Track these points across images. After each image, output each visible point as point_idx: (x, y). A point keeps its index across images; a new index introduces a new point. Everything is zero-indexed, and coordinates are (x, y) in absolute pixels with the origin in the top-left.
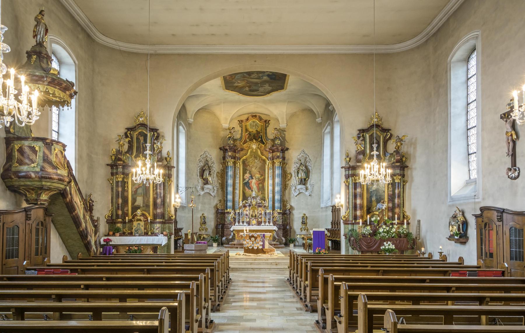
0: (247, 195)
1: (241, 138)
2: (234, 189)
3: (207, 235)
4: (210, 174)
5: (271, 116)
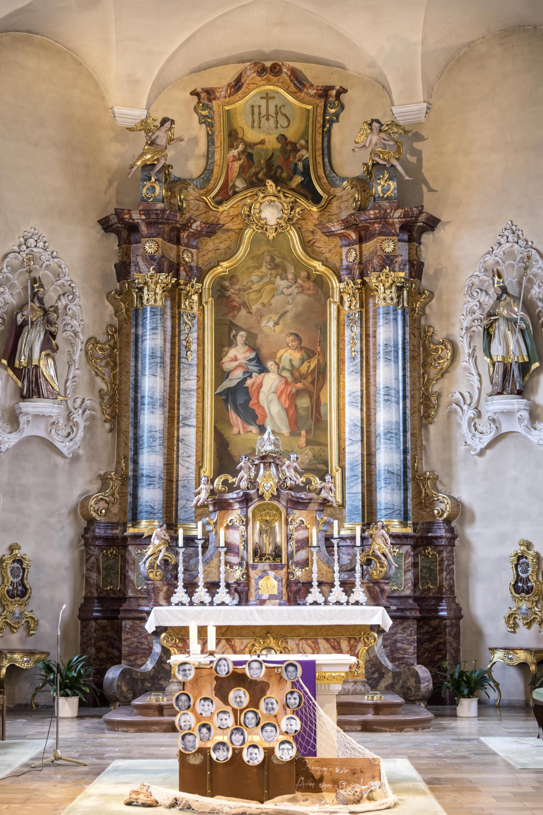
1: (208, 172)
2: (173, 420)
3: (30, 653)
4: (49, 344)
5: (352, 67)
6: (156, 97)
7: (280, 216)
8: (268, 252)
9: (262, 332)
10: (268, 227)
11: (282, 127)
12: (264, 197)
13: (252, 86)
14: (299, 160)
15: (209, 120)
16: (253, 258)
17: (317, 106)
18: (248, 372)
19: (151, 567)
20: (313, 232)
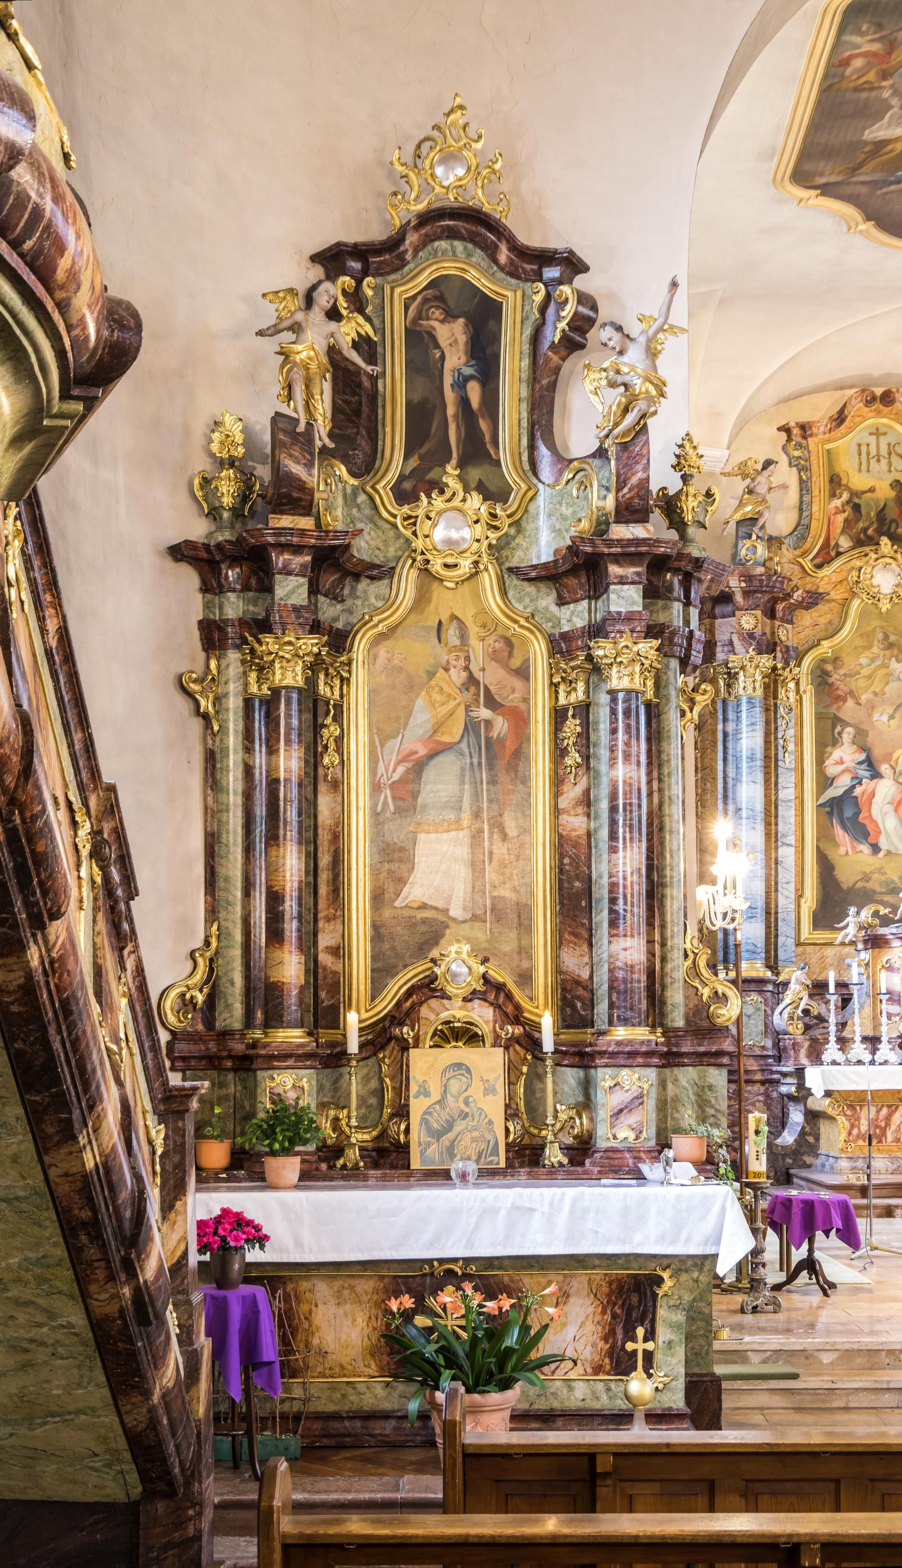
0: (846, 876)
1: (801, 530)
6: (737, 434)
8: (881, 627)
9: (874, 728)
12: (877, 559)
13: (858, 419)
16: (862, 635)
18: (857, 778)
19: (791, 1018)
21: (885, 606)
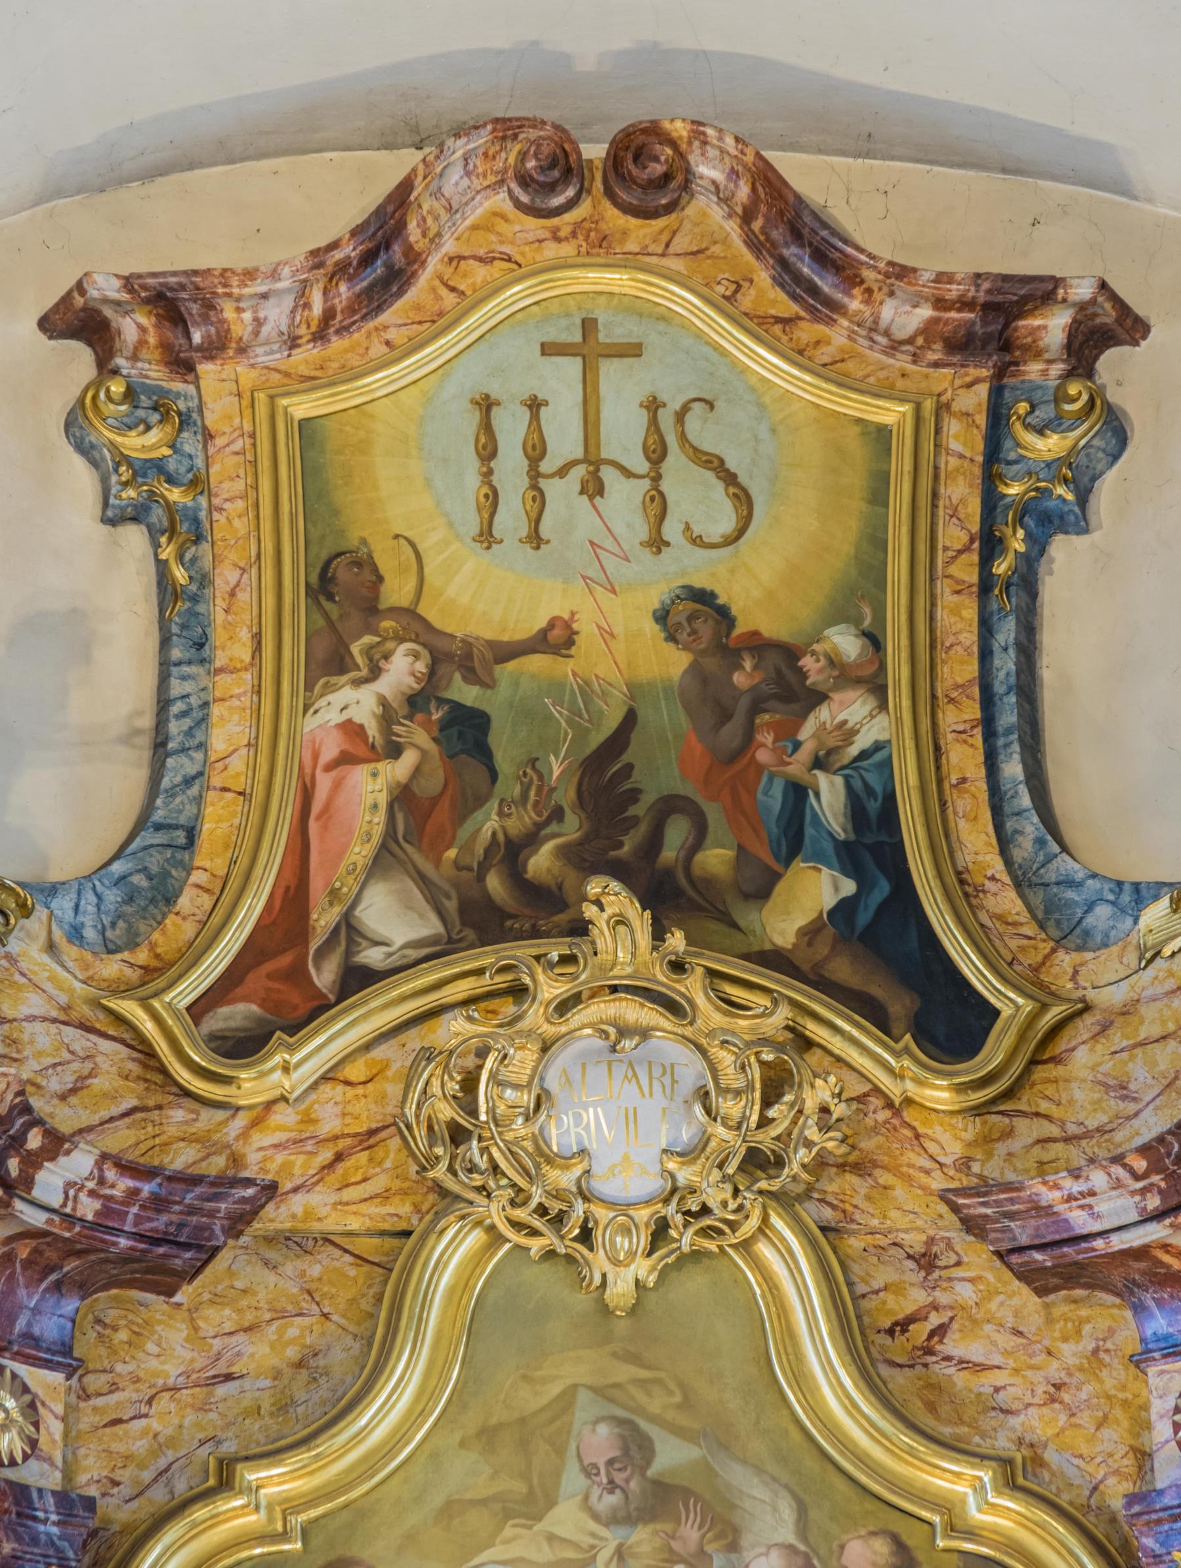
7: (687, 1136)
10: (602, 1214)
11: (697, 541)
12: (564, 1006)
13: (480, 273)
14: (819, 763)
15: (175, 495)
16: (488, 1436)
17: (942, 408)
20: (926, 1261)
21: (623, 1269)
